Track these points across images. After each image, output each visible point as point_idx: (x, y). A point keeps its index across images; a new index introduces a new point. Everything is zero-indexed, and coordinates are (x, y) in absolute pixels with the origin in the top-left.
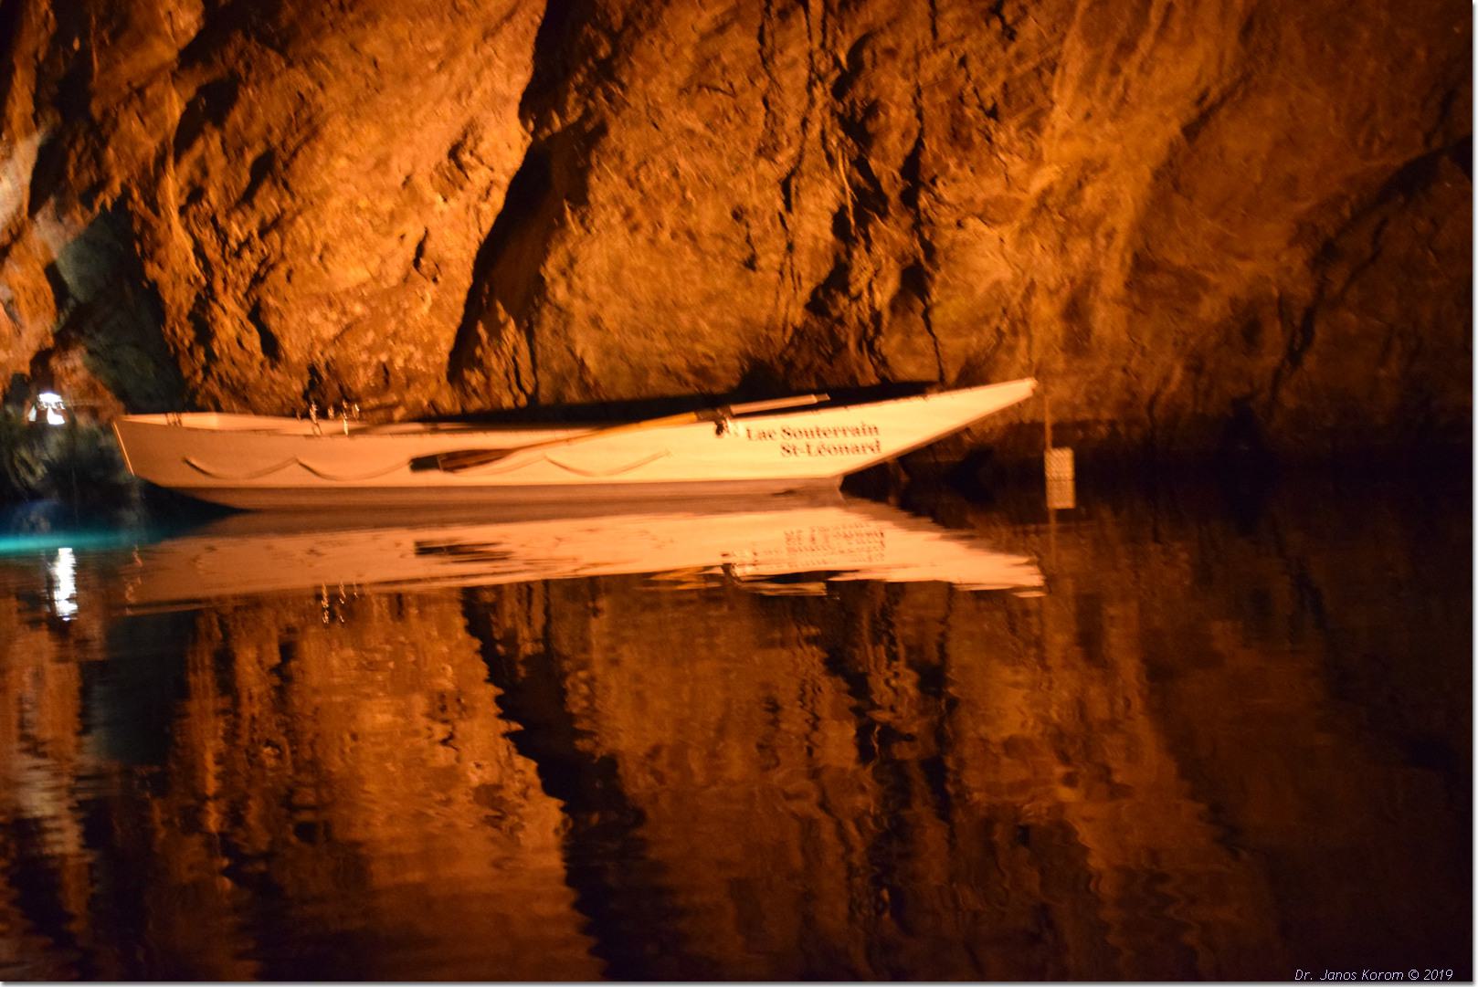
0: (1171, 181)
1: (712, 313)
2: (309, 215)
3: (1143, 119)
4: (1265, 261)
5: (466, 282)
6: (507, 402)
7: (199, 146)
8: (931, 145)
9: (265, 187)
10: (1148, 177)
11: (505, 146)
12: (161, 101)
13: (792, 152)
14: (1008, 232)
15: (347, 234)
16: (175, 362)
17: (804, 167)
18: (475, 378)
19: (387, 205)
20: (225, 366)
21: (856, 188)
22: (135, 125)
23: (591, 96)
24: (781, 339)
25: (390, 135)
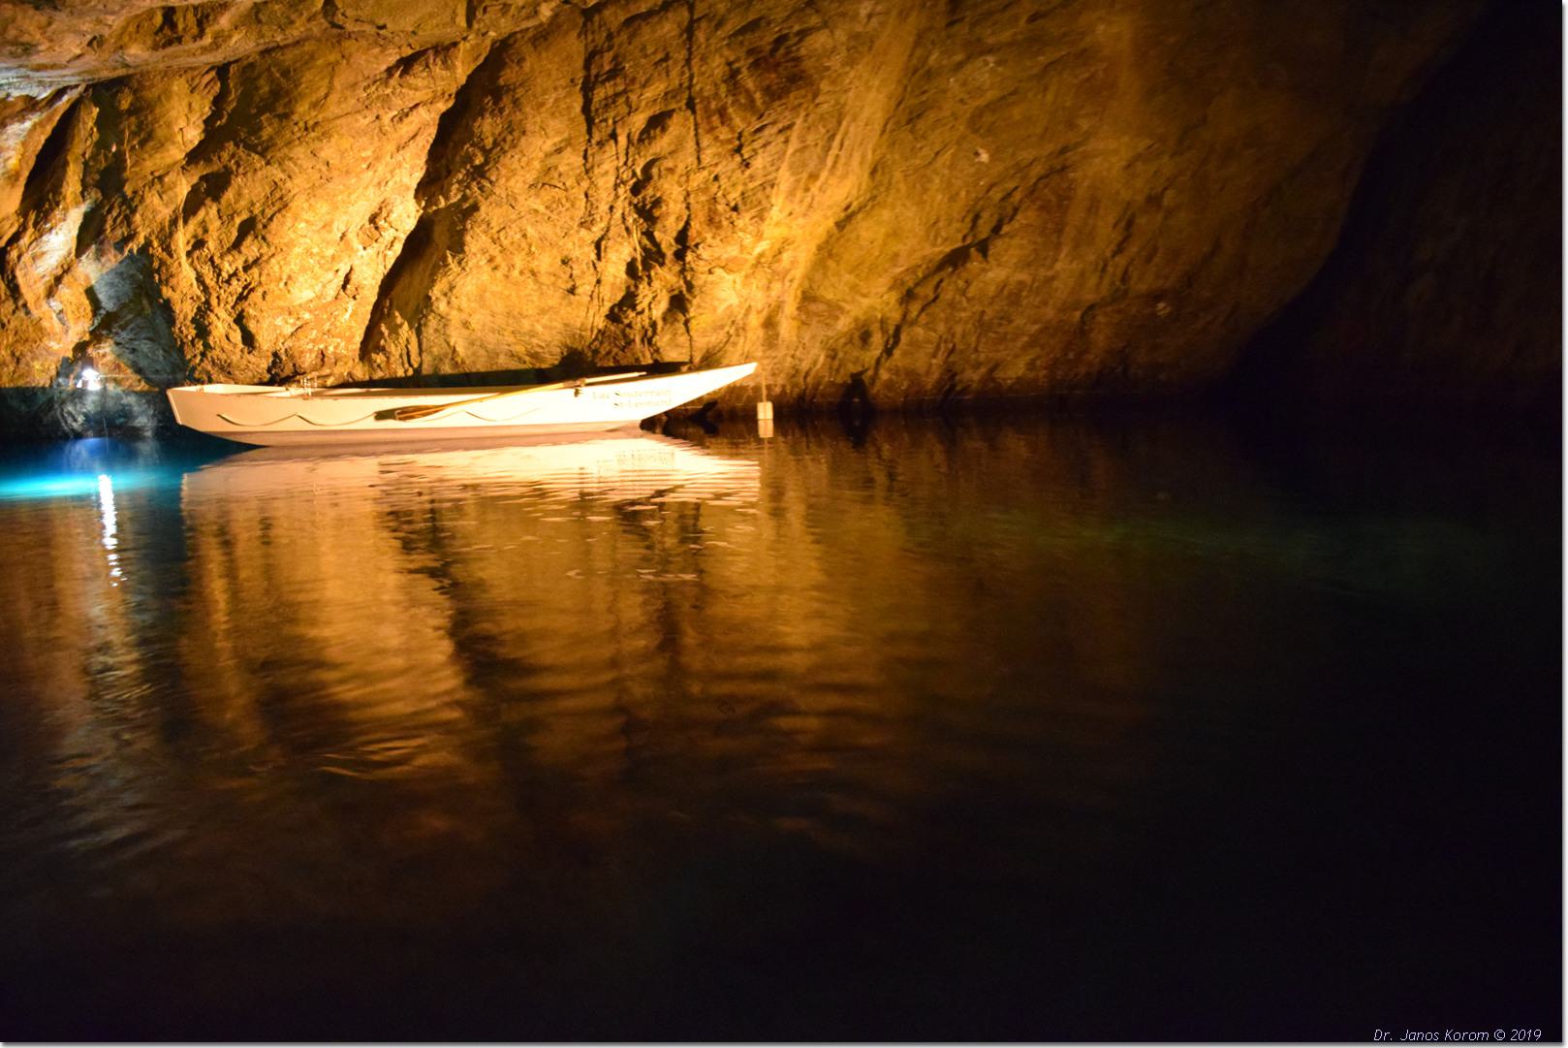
0: (827, 252)
1: (545, 320)
2: (279, 257)
3: (816, 216)
4: (877, 299)
5: (374, 299)
6: (400, 373)
7: (201, 213)
8: (695, 225)
9: (249, 239)
10: (814, 249)
11: (406, 215)
12: (175, 184)
13: (603, 225)
14: (739, 277)
15: (303, 270)
16: (181, 350)
17: (611, 234)
18: (379, 358)
19: (330, 252)
20: (216, 353)
21: (644, 249)
22: (156, 200)
23: (468, 187)
24: (589, 336)
25: (335, 208)
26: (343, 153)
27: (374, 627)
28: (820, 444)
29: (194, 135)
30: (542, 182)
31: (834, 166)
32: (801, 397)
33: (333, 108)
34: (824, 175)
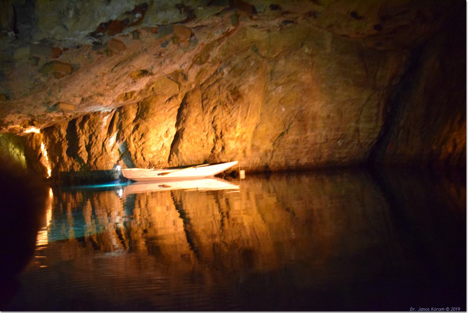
0: (255, 134)
5: (170, 149)
11: (173, 131)
15: (153, 144)
19: (158, 140)
20: (138, 162)
25: (158, 130)
26: (158, 119)
27: (168, 223)
28: (260, 181)
29: (134, 117)
30: (196, 123)
31: (250, 115)
32: (256, 169)
33: (156, 110)
34: (248, 117)
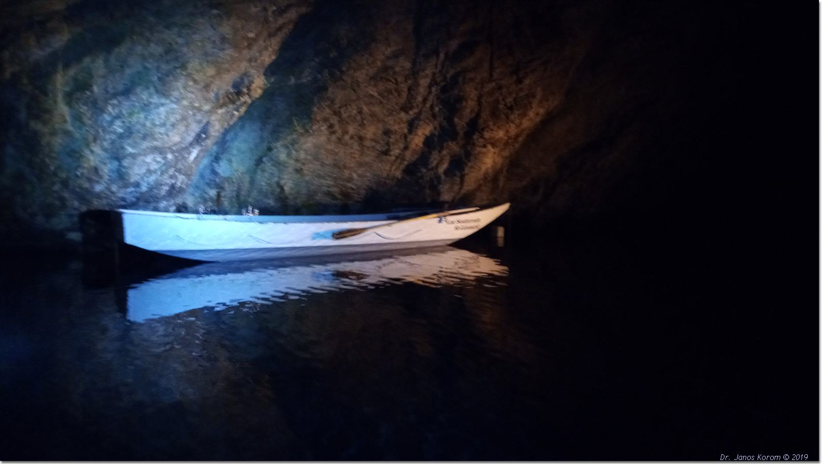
13: (416, 110)
17: (422, 117)
